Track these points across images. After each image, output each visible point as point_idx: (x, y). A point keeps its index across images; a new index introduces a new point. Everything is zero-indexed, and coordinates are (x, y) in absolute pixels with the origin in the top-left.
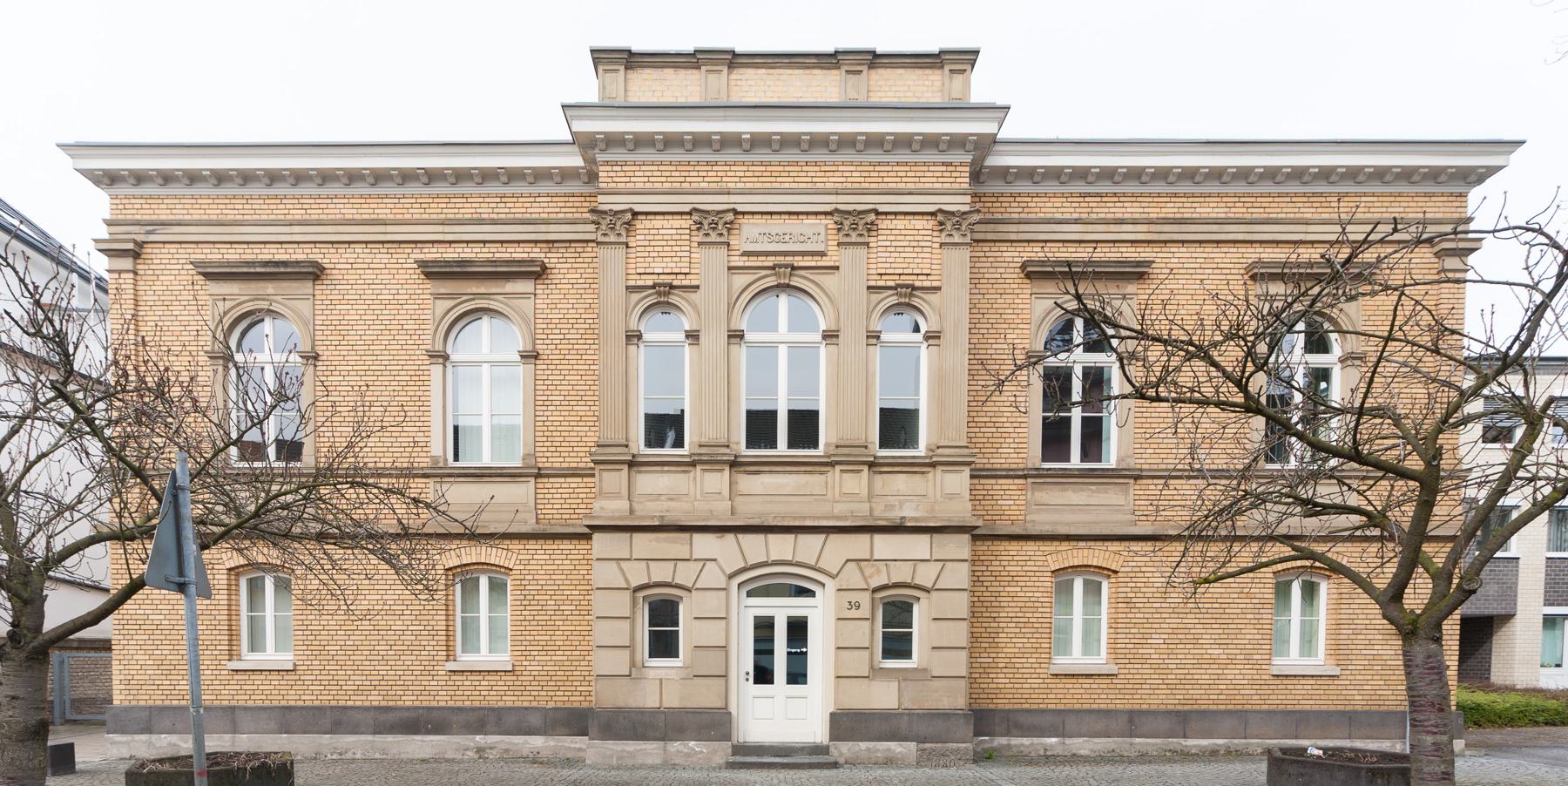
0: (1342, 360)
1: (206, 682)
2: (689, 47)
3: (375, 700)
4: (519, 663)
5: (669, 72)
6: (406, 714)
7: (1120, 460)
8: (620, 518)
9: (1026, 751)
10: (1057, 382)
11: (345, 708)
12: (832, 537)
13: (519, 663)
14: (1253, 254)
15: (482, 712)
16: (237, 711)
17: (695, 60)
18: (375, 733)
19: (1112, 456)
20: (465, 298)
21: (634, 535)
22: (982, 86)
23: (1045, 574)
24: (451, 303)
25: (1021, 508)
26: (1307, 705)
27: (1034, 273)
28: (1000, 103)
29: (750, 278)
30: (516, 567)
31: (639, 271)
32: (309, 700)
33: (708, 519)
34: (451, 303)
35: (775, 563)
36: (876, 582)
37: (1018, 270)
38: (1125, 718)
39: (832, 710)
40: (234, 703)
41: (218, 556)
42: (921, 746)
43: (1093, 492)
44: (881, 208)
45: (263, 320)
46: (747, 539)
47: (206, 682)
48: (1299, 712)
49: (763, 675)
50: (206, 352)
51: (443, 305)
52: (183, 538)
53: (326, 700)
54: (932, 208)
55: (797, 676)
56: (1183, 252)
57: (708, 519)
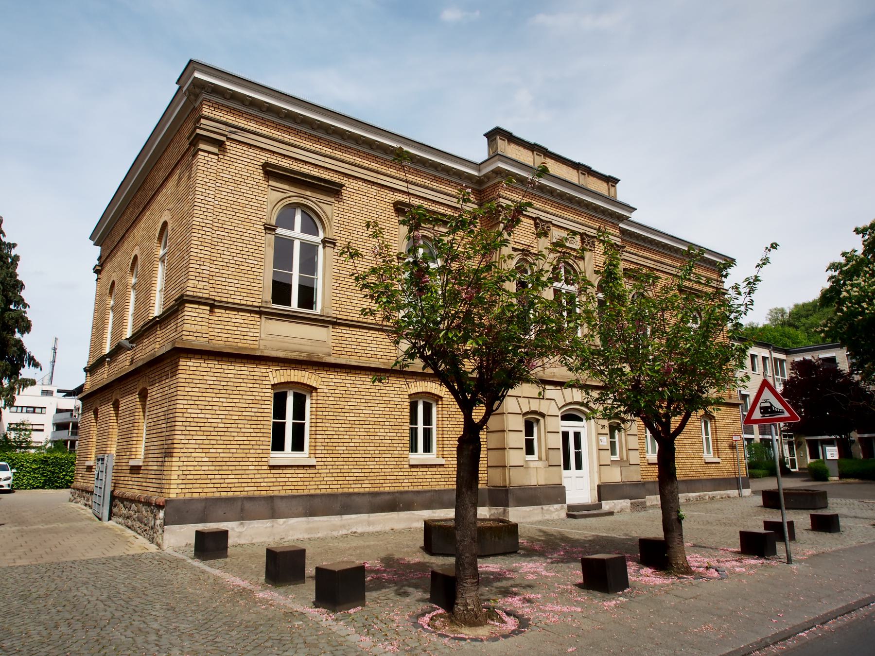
0: (324, 242)
2: (607, 174)
3: (366, 487)
5: (521, 149)
6: (387, 497)
7: (322, 310)
10: (283, 248)
11: (350, 495)
14: (265, 157)
15: (428, 495)
17: (534, 148)
19: (318, 309)
22: (622, 193)
23: (267, 387)
25: (255, 335)
27: (271, 172)
28: (632, 205)
31: (516, 240)
32: (324, 489)
33: (553, 377)
35: (570, 403)
37: (392, 205)
40: (270, 493)
41: (266, 374)
42: (633, 501)
44: (554, 222)
49: (567, 467)
52: (348, 371)
53: (336, 488)
54: (534, 216)
55: (579, 466)
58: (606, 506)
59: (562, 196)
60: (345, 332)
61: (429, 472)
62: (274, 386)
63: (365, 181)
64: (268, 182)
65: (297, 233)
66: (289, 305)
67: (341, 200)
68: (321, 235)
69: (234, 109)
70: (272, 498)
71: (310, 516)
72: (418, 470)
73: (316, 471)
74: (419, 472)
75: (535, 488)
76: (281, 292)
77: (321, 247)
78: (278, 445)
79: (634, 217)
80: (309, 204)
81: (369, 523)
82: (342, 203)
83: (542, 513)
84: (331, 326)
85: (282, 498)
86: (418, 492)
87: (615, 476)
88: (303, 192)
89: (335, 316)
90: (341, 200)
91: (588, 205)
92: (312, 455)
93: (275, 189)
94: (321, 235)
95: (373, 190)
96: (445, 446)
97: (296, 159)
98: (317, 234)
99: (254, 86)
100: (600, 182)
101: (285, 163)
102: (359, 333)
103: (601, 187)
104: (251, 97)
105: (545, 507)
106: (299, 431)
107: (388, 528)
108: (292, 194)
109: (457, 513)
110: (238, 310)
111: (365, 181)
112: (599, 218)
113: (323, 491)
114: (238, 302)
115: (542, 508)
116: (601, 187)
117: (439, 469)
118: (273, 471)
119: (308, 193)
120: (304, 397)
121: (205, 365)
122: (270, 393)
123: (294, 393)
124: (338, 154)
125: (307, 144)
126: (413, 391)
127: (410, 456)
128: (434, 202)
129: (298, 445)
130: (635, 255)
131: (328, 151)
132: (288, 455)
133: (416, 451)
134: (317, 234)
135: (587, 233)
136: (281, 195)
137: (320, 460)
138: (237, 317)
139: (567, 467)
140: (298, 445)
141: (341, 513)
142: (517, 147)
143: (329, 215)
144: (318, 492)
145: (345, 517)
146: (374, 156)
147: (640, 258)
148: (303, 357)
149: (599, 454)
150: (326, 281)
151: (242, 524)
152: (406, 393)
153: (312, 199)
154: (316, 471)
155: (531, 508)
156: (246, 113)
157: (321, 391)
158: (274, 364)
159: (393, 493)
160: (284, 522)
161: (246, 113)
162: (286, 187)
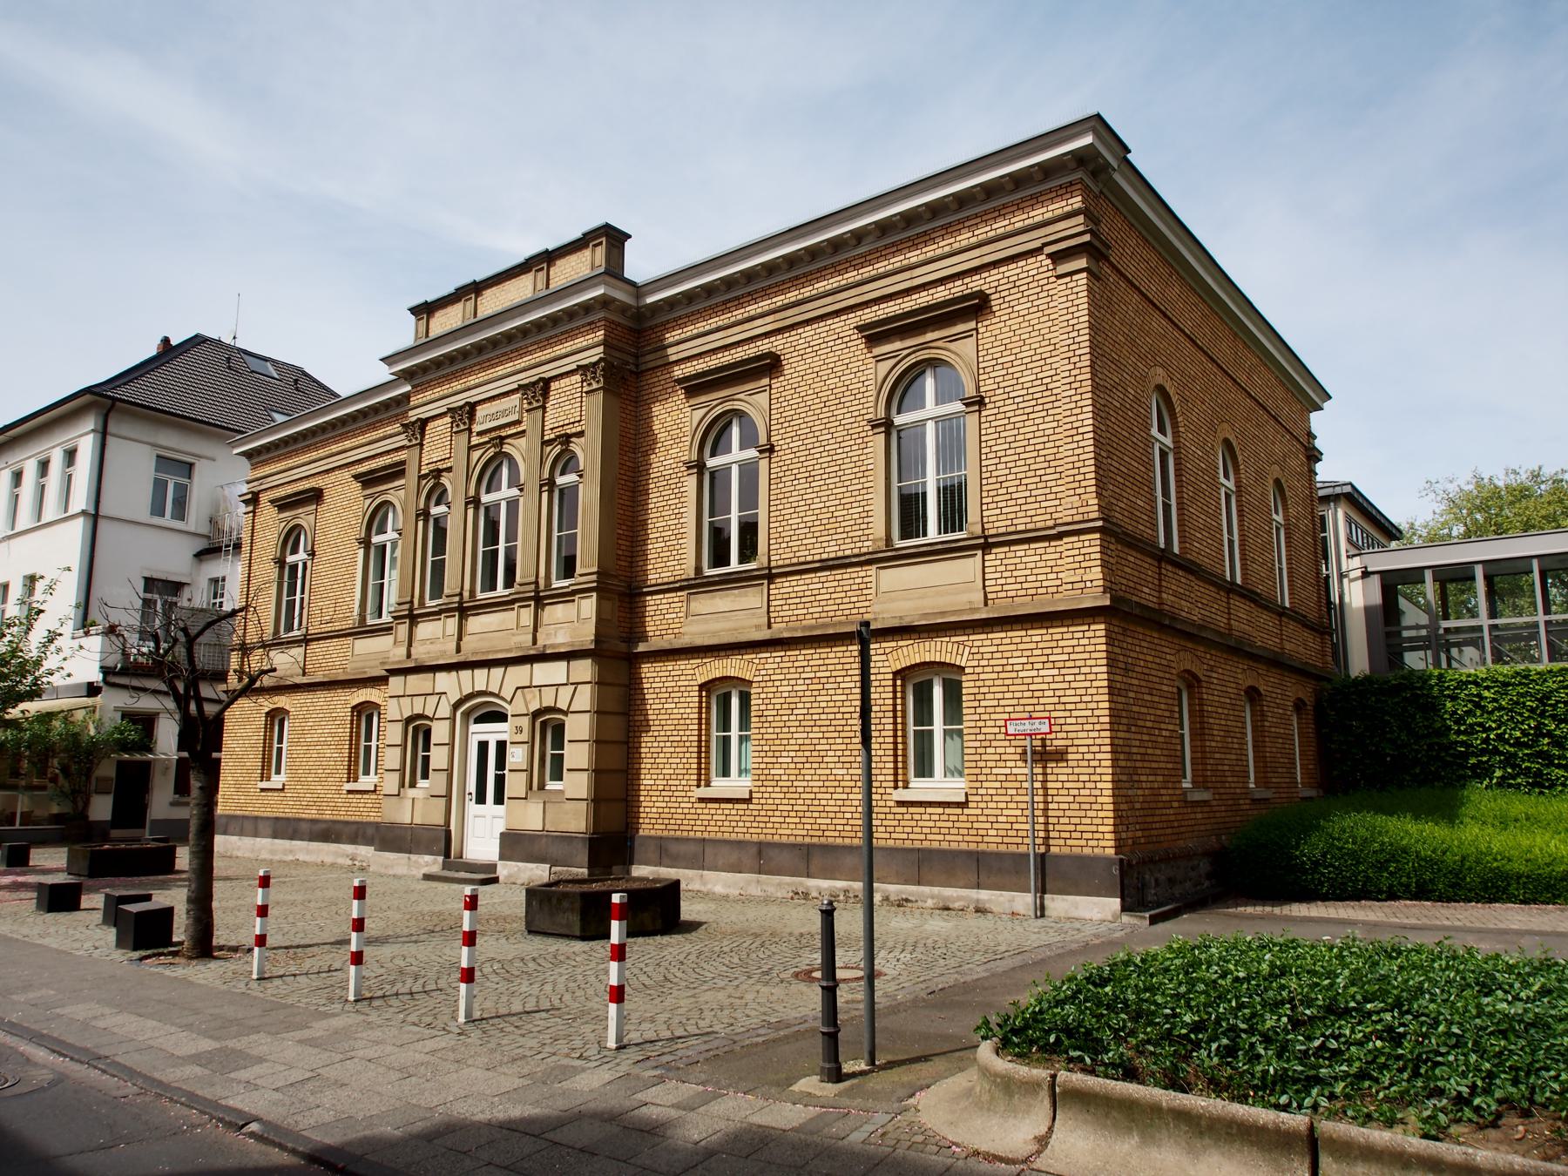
1: (880, 816)
3: (312, 813)
4: (974, 791)
6: (324, 826)
8: (399, 662)
9: (1458, 944)
12: (511, 669)
13: (974, 791)
14: (854, 319)
16: (260, 822)
18: (310, 840)
20: (715, 403)
21: (476, 671)
24: (892, 362)
26: (935, 842)
27: (875, 335)
29: (481, 451)
30: (969, 664)
33: (438, 659)
34: (892, 362)
36: (534, 706)
38: (754, 850)
39: (503, 829)
43: (736, 596)
45: (924, 372)
46: (465, 674)
47: (880, 816)
48: (357, 823)
49: (481, 799)
50: (869, 421)
51: (699, 413)
56: (807, 331)
57: (438, 659)
63: (339, 467)
69: (1004, 206)
76: (910, 512)
81: (308, 852)
86: (347, 823)
88: (921, 340)
91: (524, 331)
102: (845, 576)
104: (895, 215)
105: (414, 857)
108: (714, 403)
126: (354, 702)
128: (700, 355)
139: (481, 799)
141: (292, 838)
145: (294, 842)
147: (730, 331)
148: (896, 623)
152: (889, 670)
162: (898, 345)
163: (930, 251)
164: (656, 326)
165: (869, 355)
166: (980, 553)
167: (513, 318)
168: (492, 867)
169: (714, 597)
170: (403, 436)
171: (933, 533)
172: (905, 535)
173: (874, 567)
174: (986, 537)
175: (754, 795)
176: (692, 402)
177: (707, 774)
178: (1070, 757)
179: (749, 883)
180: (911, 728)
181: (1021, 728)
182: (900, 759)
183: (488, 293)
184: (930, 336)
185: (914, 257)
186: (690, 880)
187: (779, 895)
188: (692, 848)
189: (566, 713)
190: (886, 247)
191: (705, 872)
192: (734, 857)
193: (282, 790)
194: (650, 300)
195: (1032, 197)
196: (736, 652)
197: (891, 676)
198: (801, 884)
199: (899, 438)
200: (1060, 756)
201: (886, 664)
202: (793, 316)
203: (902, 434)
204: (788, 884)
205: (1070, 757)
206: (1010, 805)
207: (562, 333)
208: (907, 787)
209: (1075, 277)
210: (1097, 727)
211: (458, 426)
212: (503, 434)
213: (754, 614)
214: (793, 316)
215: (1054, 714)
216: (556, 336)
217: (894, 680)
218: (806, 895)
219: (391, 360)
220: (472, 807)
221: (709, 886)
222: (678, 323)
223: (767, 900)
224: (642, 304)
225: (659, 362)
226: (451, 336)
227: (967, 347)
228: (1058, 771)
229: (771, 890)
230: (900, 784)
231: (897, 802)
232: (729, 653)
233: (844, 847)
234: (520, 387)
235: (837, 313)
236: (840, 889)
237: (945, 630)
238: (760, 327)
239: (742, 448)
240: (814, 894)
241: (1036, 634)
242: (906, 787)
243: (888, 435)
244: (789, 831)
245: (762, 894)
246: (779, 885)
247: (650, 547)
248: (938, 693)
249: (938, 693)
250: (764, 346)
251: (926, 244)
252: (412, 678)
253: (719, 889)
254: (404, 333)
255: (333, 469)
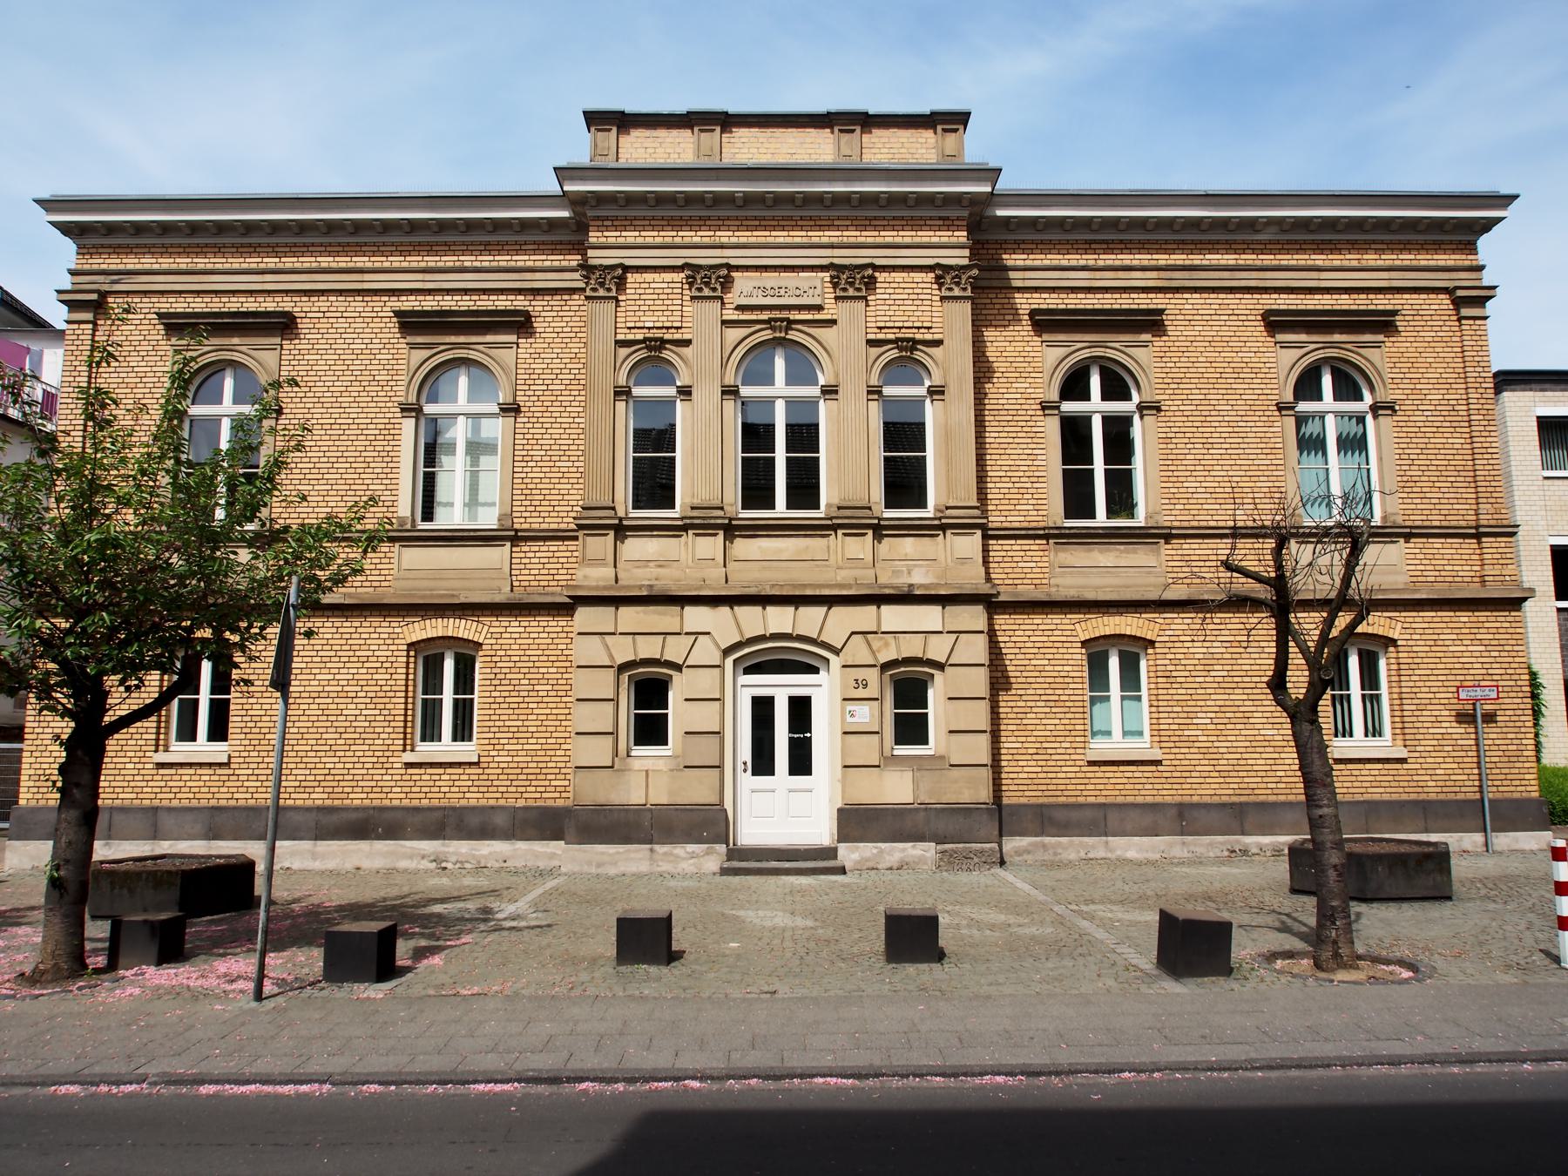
1: (108, 778)
3: (318, 798)
4: (486, 753)
6: (354, 816)
7: (1384, 518)
8: (605, 588)
10: (1075, 435)
16: (160, 813)
18: (316, 838)
20: (1079, 345)
26: (1377, 794)
27: (1275, 323)
31: (629, 325)
38: (1174, 811)
39: (840, 805)
43: (1121, 552)
44: (878, 262)
54: (680, 262)
55: (801, 763)
58: (849, 854)
59: (750, 200)
60: (1196, 546)
61: (447, 775)
62: (1084, 643)
63: (341, 292)
64: (1273, 337)
65: (1096, 405)
66: (1093, 517)
67: (297, 335)
68: (1368, 399)
69: (120, 246)
70: (156, 809)
71: (214, 838)
72: (422, 771)
73: (231, 772)
74: (426, 775)
75: (639, 810)
77: (1136, 418)
78: (431, 732)
79: (1004, 184)
80: (1111, 354)
81: (314, 856)
82: (297, 341)
83: (651, 859)
84: (1402, 540)
85: (170, 809)
86: (416, 809)
87: (896, 789)
89: (1168, 524)
90: (297, 335)
92: (1156, 744)
93: (1285, 346)
94: (1368, 399)
95: (357, 304)
96: (1406, 725)
97: (216, 292)
98: (1360, 398)
99: (152, 204)
100: (675, 132)
101: (198, 305)
103: (920, 148)
105: (660, 849)
106: (463, 712)
107: (349, 865)
108: (1080, 347)
109: (89, 851)
110: (545, 539)
111: (341, 292)
112: (894, 218)
113: (242, 803)
114: (1204, 524)
115: (651, 850)
116: (920, 148)
117: (467, 771)
118: (161, 772)
119: (236, 340)
120: (1138, 655)
121: (555, 623)
122: (1079, 656)
123: (1120, 651)
124: (289, 262)
125: (236, 263)
127: (1335, 744)
128: (485, 291)
129: (462, 731)
130: (1084, 268)
131: (271, 262)
132: (446, 747)
133: (194, 739)
134: (1360, 398)
135: (836, 261)
136: (1062, 352)
137: (1167, 751)
138: (1015, 548)
140: (462, 731)
142: (648, 133)
143: (1378, 365)
144: (232, 803)
146: (1210, 242)
147: (1098, 274)
149: (843, 741)
150: (1385, 470)
151: (107, 844)
152: (403, 642)
153: (1116, 347)
154: (231, 772)
155: (621, 848)
156: (137, 246)
157: (1404, 643)
158: (485, 613)
159: (365, 809)
160: (171, 846)
161: (137, 246)
162: (1303, 337)
163: (1336, 260)
164: (987, 242)
165: (401, 340)
166: (509, 544)
167: (861, 180)
168: (831, 853)
169: (1090, 551)
170: (577, 275)
171: (1101, 518)
172: (424, 519)
173: (397, 545)
174: (517, 531)
175: (233, 760)
176: (410, 339)
177: (166, 740)
178: (1499, 718)
179: (1171, 845)
180: (420, 696)
181: (1473, 694)
182: (163, 725)
183: (741, 134)
184: (1337, 337)
185: (1319, 260)
186: (1461, 842)
187: (1211, 854)
188: (1089, 813)
189: (678, 668)
190: (1289, 242)
191: (1110, 838)
192: (1148, 819)
193: (227, 765)
194: (1000, 213)
195: (1434, 242)
196: (1133, 610)
197: (405, 647)
198: (1238, 842)
199: (191, 426)
200: (1490, 718)
201: (1074, 633)
202: (1180, 278)
203: (194, 423)
204: (1221, 843)
205: (1499, 718)
206: (357, 766)
207: (894, 218)
208: (412, 751)
209: (82, 326)
210: (1520, 695)
211: (700, 290)
212: (792, 317)
213: (1149, 573)
214: (1180, 278)
215: (1501, 683)
216: (884, 218)
217: (408, 651)
218: (1245, 852)
219: (566, 173)
220: (748, 781)
221: (1119, 853)
222: (1018, 246)
223: (1198, 861)
224: (989, 213)
225: (995, 283)
226: (713, 173)
227: (507, 356)
228: (1491, 734)
229: (1200, 850)
230: (408, 748)
231: (157, 764)
232: (1121, 610)
233: (1284, 804)
234: (938, 265)
235: (1231, 290)
236: (1284, 844)
237: (1005, 607)
238: (1150, 279)
239: (236, 401)
240: (1255, 850)
241: (1464, 617)
242: (166, 750)
243: (417, 419)
244: (1208, 789)
245: (1190, 855)
246: (1211, 844)
247: (989, 485)
248: (449, 666)
249: (449, 666)
250: (286, 305)
251: (1332, 251)
252: (771, 610)
253: (1131, 854)
254: (579, 147)
255: (323, 292)
